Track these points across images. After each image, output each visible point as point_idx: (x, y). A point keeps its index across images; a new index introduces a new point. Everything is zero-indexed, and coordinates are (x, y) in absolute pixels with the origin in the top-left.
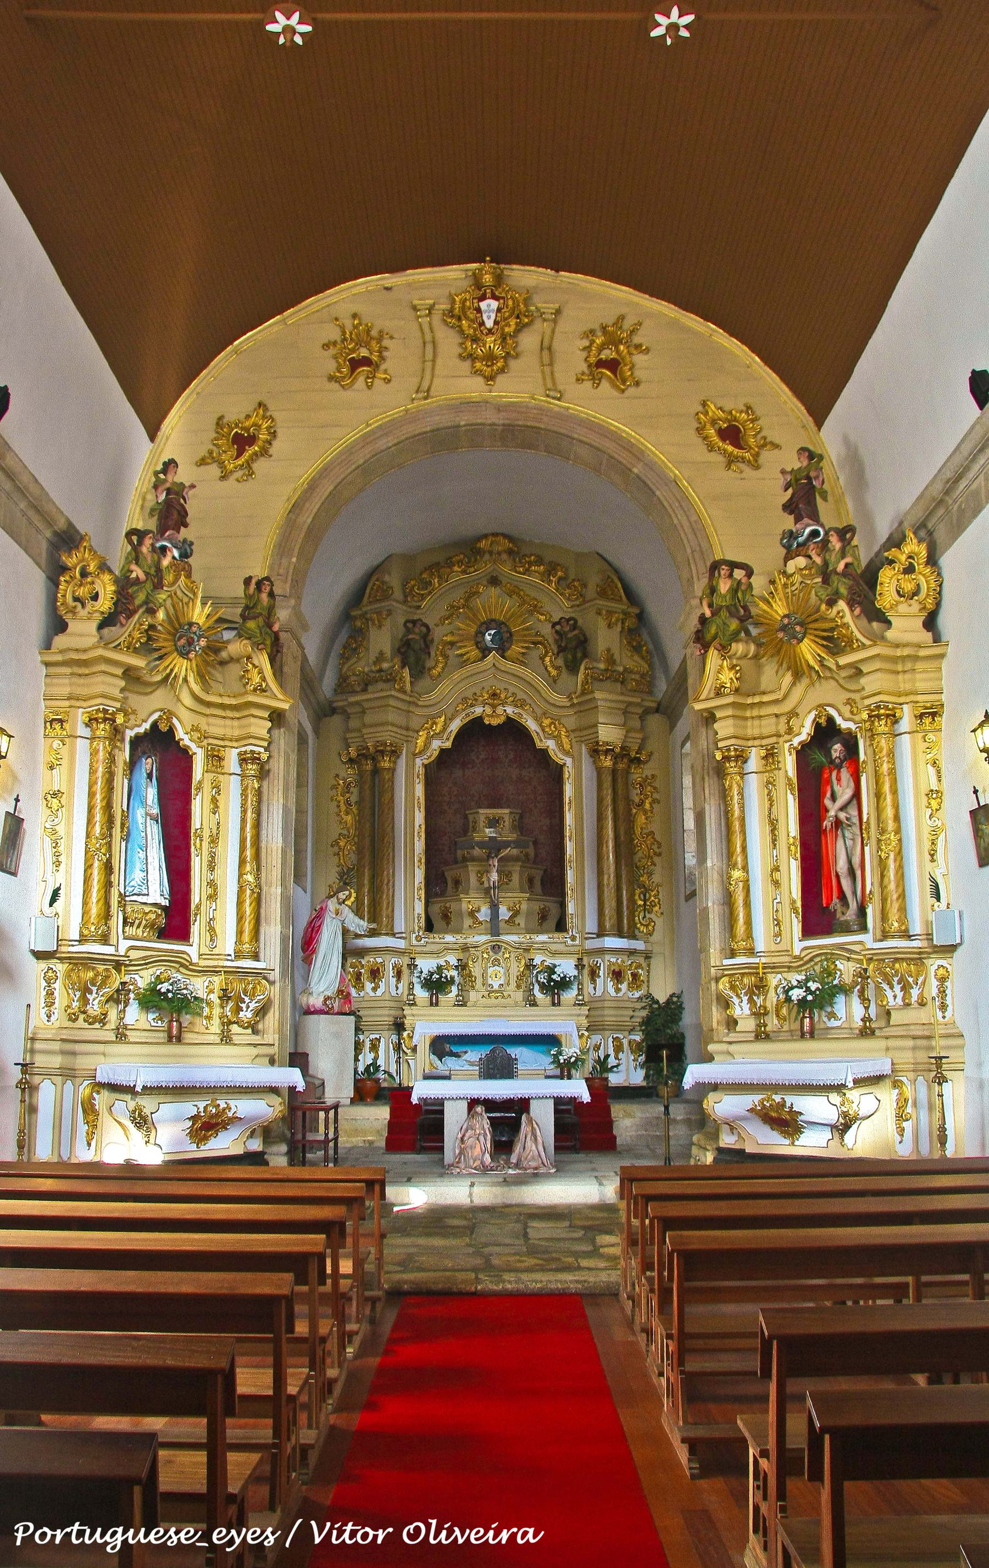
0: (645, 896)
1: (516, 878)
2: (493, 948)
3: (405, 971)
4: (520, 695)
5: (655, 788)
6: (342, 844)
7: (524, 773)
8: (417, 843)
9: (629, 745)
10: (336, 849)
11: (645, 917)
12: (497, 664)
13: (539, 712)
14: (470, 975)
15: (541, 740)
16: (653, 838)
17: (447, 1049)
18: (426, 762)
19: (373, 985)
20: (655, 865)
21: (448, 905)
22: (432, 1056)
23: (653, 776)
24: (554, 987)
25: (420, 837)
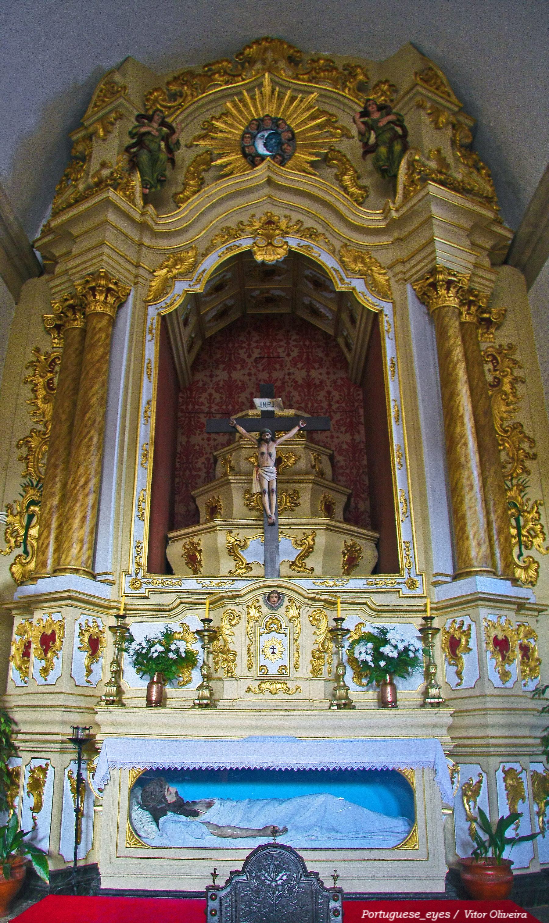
0: (517, 520)
1: (305, 500)
2: (268, 597)
3: (109, 638)
4: (309, 223)
5: (515, 362)
6: (33, 444)
7: (314, 374)
8: (141, 428)
9: (479, 287)
10: (24, 451)
11: (520, 555)
12: (274, 177)
13: (338, 245)
14: (225, 651)
15: (342, 280)
16: (521, 432)
17: (171, 799)
18: (164, 312)
19: (44, 663)
20: (528, 473)
21: (195, 540)
22: (139, 814)
23: (511, 347)
24: (386, 671)
25: (147, 418)
